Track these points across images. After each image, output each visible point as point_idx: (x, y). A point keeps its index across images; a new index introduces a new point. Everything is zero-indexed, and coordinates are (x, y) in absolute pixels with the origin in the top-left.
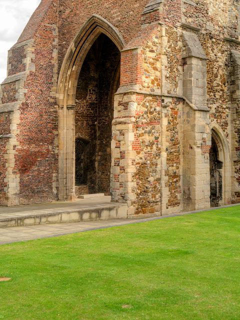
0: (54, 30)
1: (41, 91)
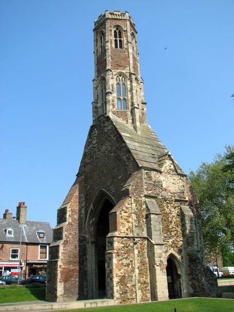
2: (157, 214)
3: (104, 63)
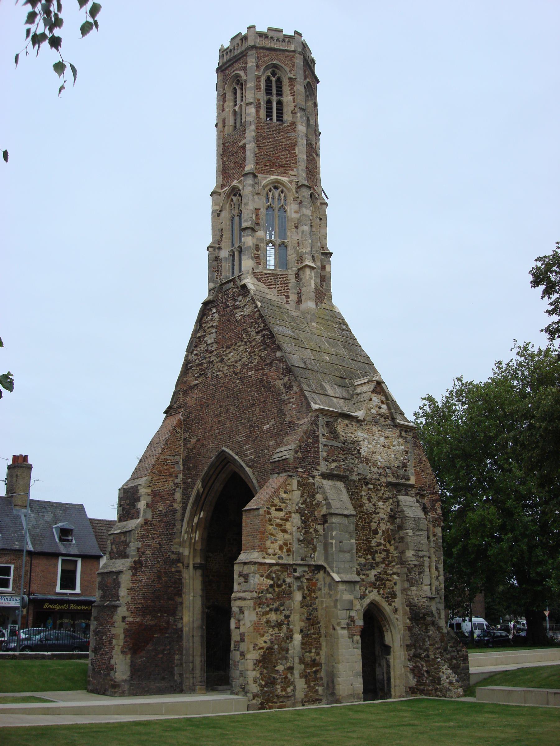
0: (177, 463)
2: (347, 516)
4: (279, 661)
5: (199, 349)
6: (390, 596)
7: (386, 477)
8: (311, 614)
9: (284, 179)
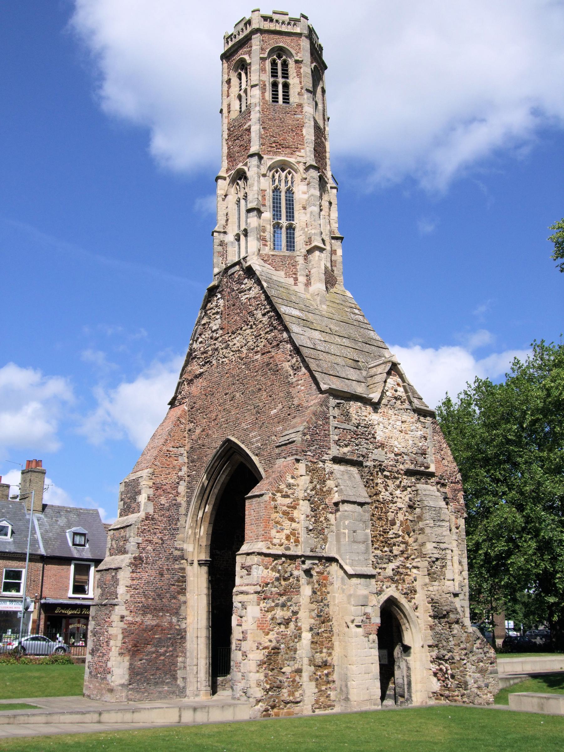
0: (182, 455)
1: (162, 540)
2: (361, 504)
3: (246, 137)
4: (286, 662)
5: (203, 337)
6: (409, 592)
7: (403, 464)
8: (321, 611)
9: (292, 160)
